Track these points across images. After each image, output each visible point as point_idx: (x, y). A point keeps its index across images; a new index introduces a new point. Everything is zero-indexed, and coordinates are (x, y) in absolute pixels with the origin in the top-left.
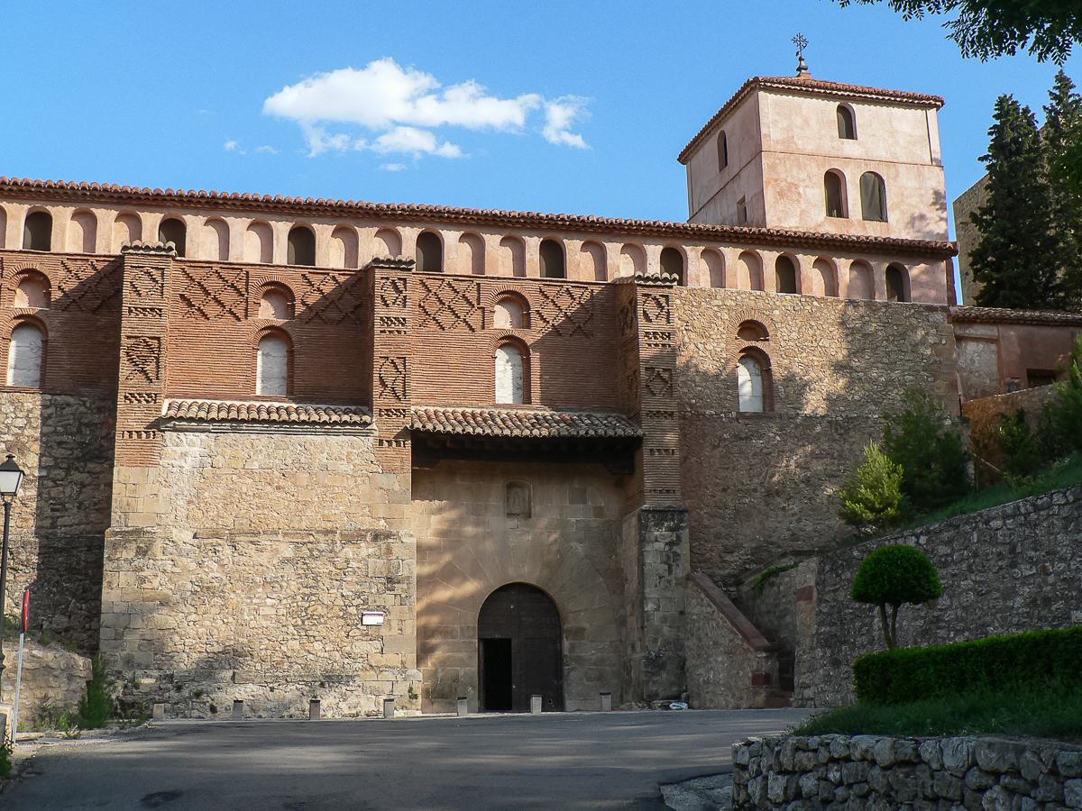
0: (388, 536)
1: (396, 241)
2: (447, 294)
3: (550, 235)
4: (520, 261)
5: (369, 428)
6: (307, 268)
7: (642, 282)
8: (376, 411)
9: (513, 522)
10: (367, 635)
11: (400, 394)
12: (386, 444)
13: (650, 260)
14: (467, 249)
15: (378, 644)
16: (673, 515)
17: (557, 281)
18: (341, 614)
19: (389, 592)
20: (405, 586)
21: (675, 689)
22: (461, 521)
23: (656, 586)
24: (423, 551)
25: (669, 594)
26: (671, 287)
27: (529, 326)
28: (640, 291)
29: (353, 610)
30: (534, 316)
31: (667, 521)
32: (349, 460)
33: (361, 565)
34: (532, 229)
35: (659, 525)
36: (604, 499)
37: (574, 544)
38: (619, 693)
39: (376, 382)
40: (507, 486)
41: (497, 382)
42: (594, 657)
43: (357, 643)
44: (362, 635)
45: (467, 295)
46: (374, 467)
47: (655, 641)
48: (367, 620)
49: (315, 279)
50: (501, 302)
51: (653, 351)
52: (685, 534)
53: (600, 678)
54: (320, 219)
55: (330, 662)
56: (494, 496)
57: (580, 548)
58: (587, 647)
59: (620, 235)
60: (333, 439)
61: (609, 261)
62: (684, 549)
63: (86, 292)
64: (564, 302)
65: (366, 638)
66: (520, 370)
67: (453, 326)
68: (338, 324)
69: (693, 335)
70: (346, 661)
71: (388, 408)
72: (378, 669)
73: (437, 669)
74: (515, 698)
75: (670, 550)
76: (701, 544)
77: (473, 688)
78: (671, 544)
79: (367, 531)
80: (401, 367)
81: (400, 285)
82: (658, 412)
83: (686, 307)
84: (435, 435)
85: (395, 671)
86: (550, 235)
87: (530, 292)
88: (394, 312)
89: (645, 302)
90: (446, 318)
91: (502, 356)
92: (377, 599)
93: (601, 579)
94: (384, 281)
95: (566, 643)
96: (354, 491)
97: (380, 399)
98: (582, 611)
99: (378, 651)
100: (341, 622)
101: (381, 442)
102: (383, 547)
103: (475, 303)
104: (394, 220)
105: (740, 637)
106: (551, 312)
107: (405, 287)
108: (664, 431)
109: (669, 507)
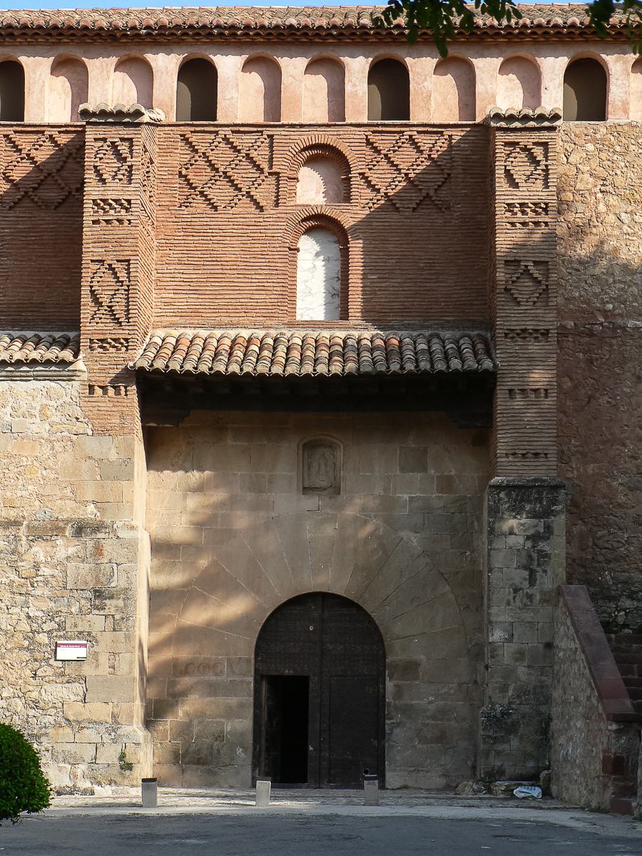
0: (98, 527)
1: (144, 75)
2: (222, 156)
3: (385, 52)
4: (337, 95)
5: (71, 368)
6: (12, 126)
7: (503, 124)
8: (84, 343)
9: (311, 502)
10: (63, 675)
11: (121, 315)
12: (99, 391)
13: (546, 81)
14: (255, 81)
15: (78, 688)
16: (540, 493)
17: (395, 126)
18: (26, 643)
19: (96, 612)
20: (121, 603)
21: (531, 764)
22: (232, 502)
23: (508, 604)
24: (161, 548)
25: (528, 616)
26: (553, 129)
27: (347, 198)
28: (501, 138)
29: (43, 638)
30: (356, 182)
31: (530, 502)
32: (44, 416)
33: (56, 572)
34: (354, 44)
35: (516, 510)
36: (455, 464)
37: (404, 534)
38: (470, 763)
39: (86, 298)
40: (305, 446)
41: (300, 287)
42: (432, 707)
43: (47, 686)
44: (55, 674)
45: (253, 154)
46: (80, 427)
47: (504, 689)
48: (63, 653)
49: (24, 142)
50: (310, 162)
51: (518, 235)
52: (559, 522)
53: (441, 738)
54: (30, 49)
55: (7, 714)
56: (284, 462)
57: (414, 540)
58: (421, 694)
59: (497, 45)
60: (20, 386)
61: (480, 88)
62: (557, 548)
63: (65, 162)
64: (406, 158)
65: (60, 680)
66: (337, 266)
67: (231, 204)
68: (56, 207)
69: (613, 200)
70: (32, 712)
71: (102, 337)
72: (77, 725)
73: (191, 721)
74: (311, 765)
75: (533, 547)
76: (610, 534)
77: (245, 750)
78: (535, 538)
79: (67, 521)
80: (122, 275)
81: (124, 148)
82: (524, 331)
83: (603, 155)
84: (172, 378)
85: (102, 728)
86: (385, 52)
87: (349, 143)
88: (114, 191)
89: (508, 155)
90: (220, 193)
91: (308, 246)
92: (79, 623)
93: (447, 588)
94: (100, 144)
95: (390, 685)
96: (50, 463)
97: (92, 323)
98: (413, 635)
99: (79, 698)
100: (26, 655)
101: (91, 388)
102: (90, 544)
103: (265, 166)
104: (139, 44)
105: (596, 694)
106: (384, 175)
107: (131, 152)
108: (532, 360)
109: (535, 480)
